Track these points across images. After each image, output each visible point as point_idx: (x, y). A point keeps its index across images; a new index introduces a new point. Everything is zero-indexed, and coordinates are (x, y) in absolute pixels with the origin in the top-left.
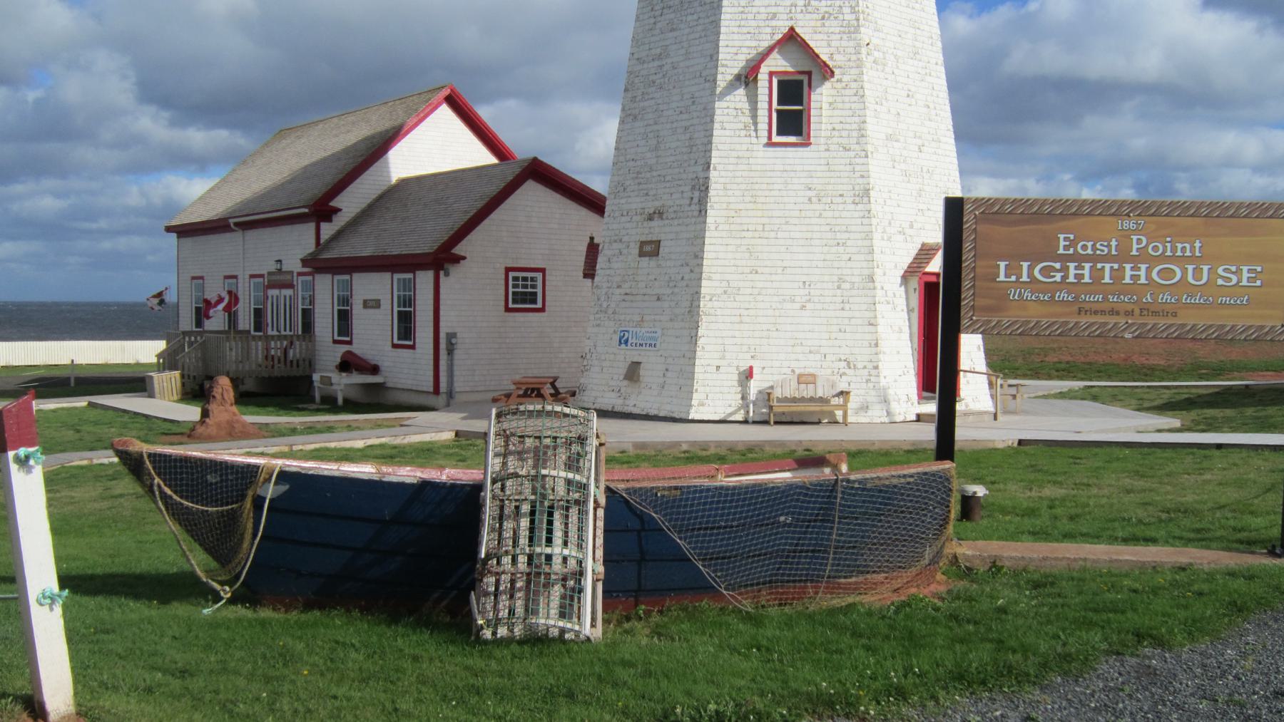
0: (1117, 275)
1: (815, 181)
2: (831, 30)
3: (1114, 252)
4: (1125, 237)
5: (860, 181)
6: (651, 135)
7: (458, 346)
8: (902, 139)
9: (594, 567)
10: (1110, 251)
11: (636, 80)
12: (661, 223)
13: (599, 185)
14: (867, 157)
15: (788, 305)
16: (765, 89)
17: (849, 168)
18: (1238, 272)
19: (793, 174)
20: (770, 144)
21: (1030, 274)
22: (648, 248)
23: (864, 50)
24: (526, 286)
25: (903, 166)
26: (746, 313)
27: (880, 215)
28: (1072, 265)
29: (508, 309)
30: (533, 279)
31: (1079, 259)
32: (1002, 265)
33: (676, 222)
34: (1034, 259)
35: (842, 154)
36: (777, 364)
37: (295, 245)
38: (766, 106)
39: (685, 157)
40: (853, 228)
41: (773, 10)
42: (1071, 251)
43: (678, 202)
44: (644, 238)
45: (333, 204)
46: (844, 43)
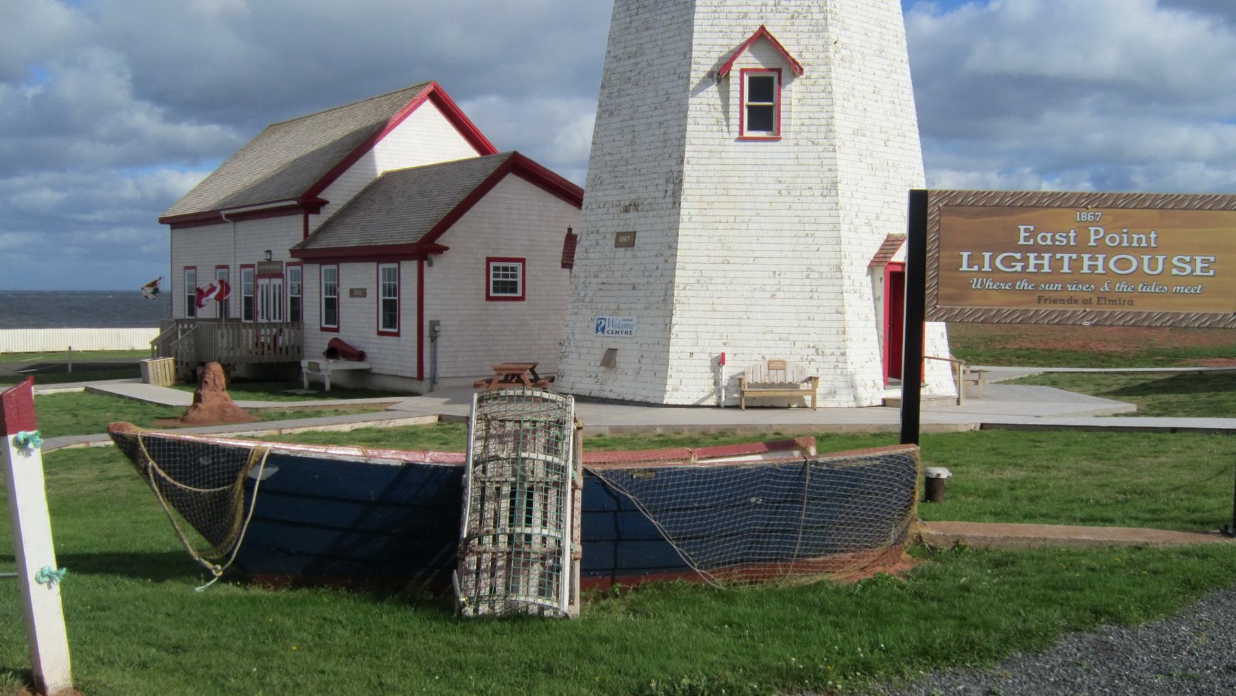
0: (1076, 265)
1: (785, 174)
2: (800, 29)
3: (1072, 243)
4: (1083, 228)
5: (828, 174)
6: (627, 130)
7: (442, 334)
8: (868, 134)
9: (572, 546)
10: (1068, 241)
11: (613, 77)
12: (636, 215)
13: (576, 178)
14: (834, 151)
15: (758, 294)
16: (737, 85)
17: (817, 162)
18: (1192, 262)
19: (763, 168)
20: (742, 139)
21: (992, 264)
22: (623, 239)
23: (832, 49)
24: (506, 276)
25: (869, 160)
26: (718, 301)
27: (848, 207)
28: (1032, 256)
29: (489, 298)
30: (513, 269)
31: (1039, 250)
32: (965, 255)
33: (651, 214)
34: (996, 250)
35: (811, 148)
36: (748, 351)
37: (284, 236)
38: (738, 102)
39: (660, 151)
40: (822, 220)
41: (745, 9)
42: (1031, 242)
43: (653, 195)
44: (620, 230)
45: (322, 196)
46: (813, 42)
